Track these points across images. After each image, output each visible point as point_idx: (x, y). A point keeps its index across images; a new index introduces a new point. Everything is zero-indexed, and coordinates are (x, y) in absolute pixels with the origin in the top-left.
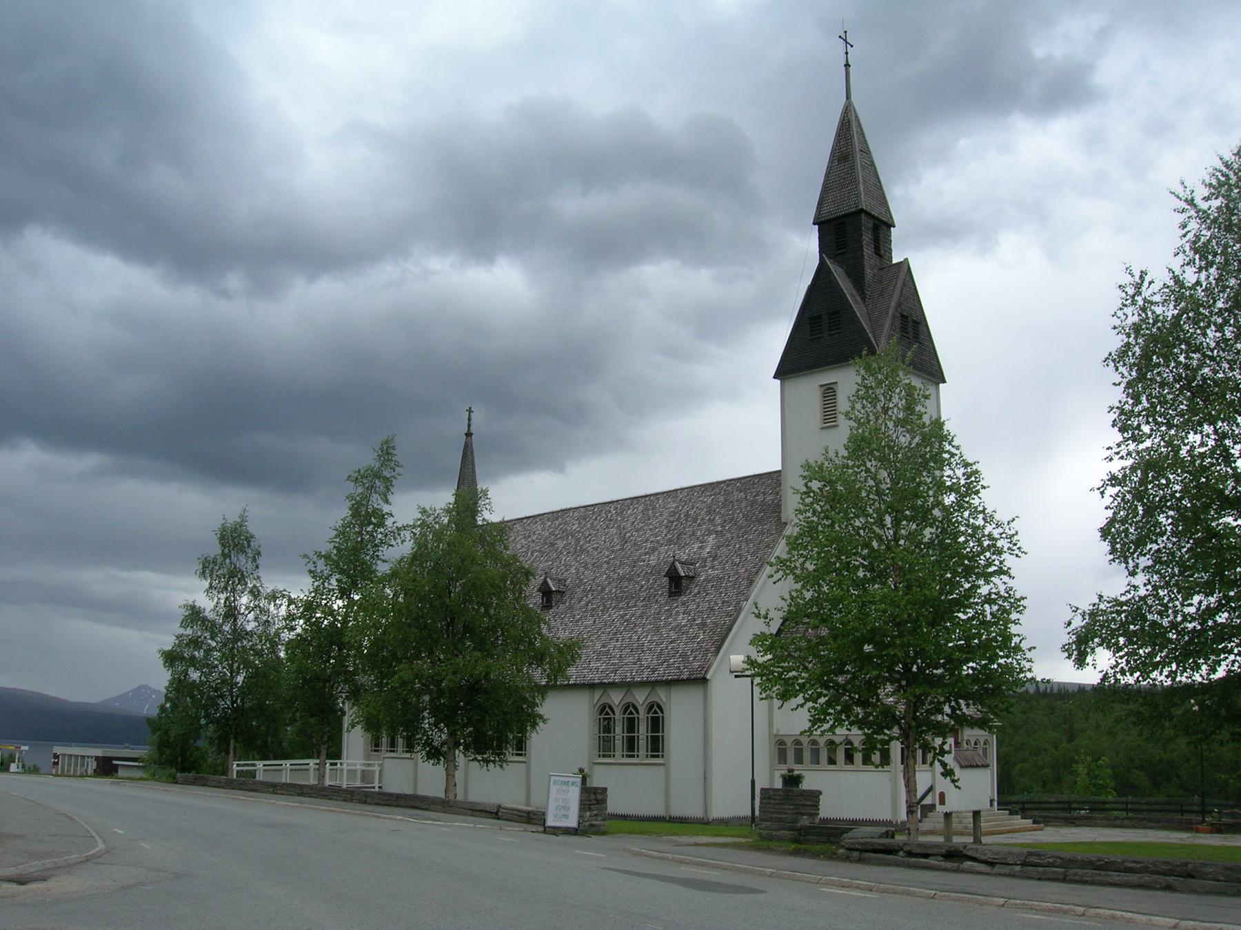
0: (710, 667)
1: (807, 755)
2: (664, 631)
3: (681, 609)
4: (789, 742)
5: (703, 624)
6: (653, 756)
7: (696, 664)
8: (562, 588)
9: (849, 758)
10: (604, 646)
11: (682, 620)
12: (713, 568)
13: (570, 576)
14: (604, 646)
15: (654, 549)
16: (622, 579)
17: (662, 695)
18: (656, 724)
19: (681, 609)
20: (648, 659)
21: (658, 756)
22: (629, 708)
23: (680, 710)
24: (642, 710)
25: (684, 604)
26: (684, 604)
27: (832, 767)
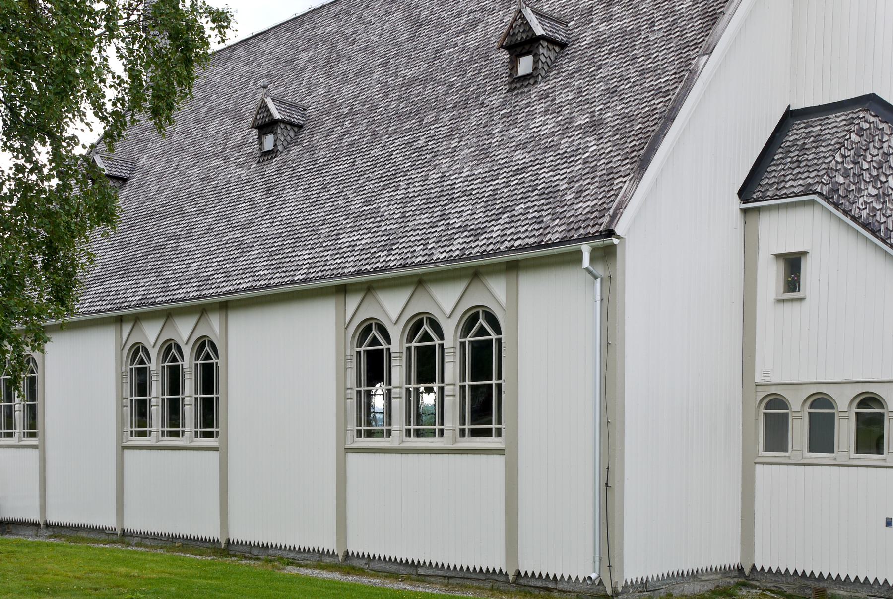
0: (622, 206)
1: (799, 430)
2: (501, 154)
3: (540, 107)
4: (796, 402)
5: (595, 125)
6: (475, 433)
7: (583, 207)
8: (297, 118)
9: (822, 437)
10: (368, 203)
11: (544, 124)
12: (609, 19)
13: (314, 102)
14: (368, 203)
15: (475, 24)
16: (408, 84)
17: (495, 293)
18: (482, 360)
19: (540, 107)
20: (464, 212)
21: (487, 433)
22: (422, 326)
23: (545, 322)
24: (450, 328)
25: (544, 96)
26: (544, 96)
27: (873, 458)
